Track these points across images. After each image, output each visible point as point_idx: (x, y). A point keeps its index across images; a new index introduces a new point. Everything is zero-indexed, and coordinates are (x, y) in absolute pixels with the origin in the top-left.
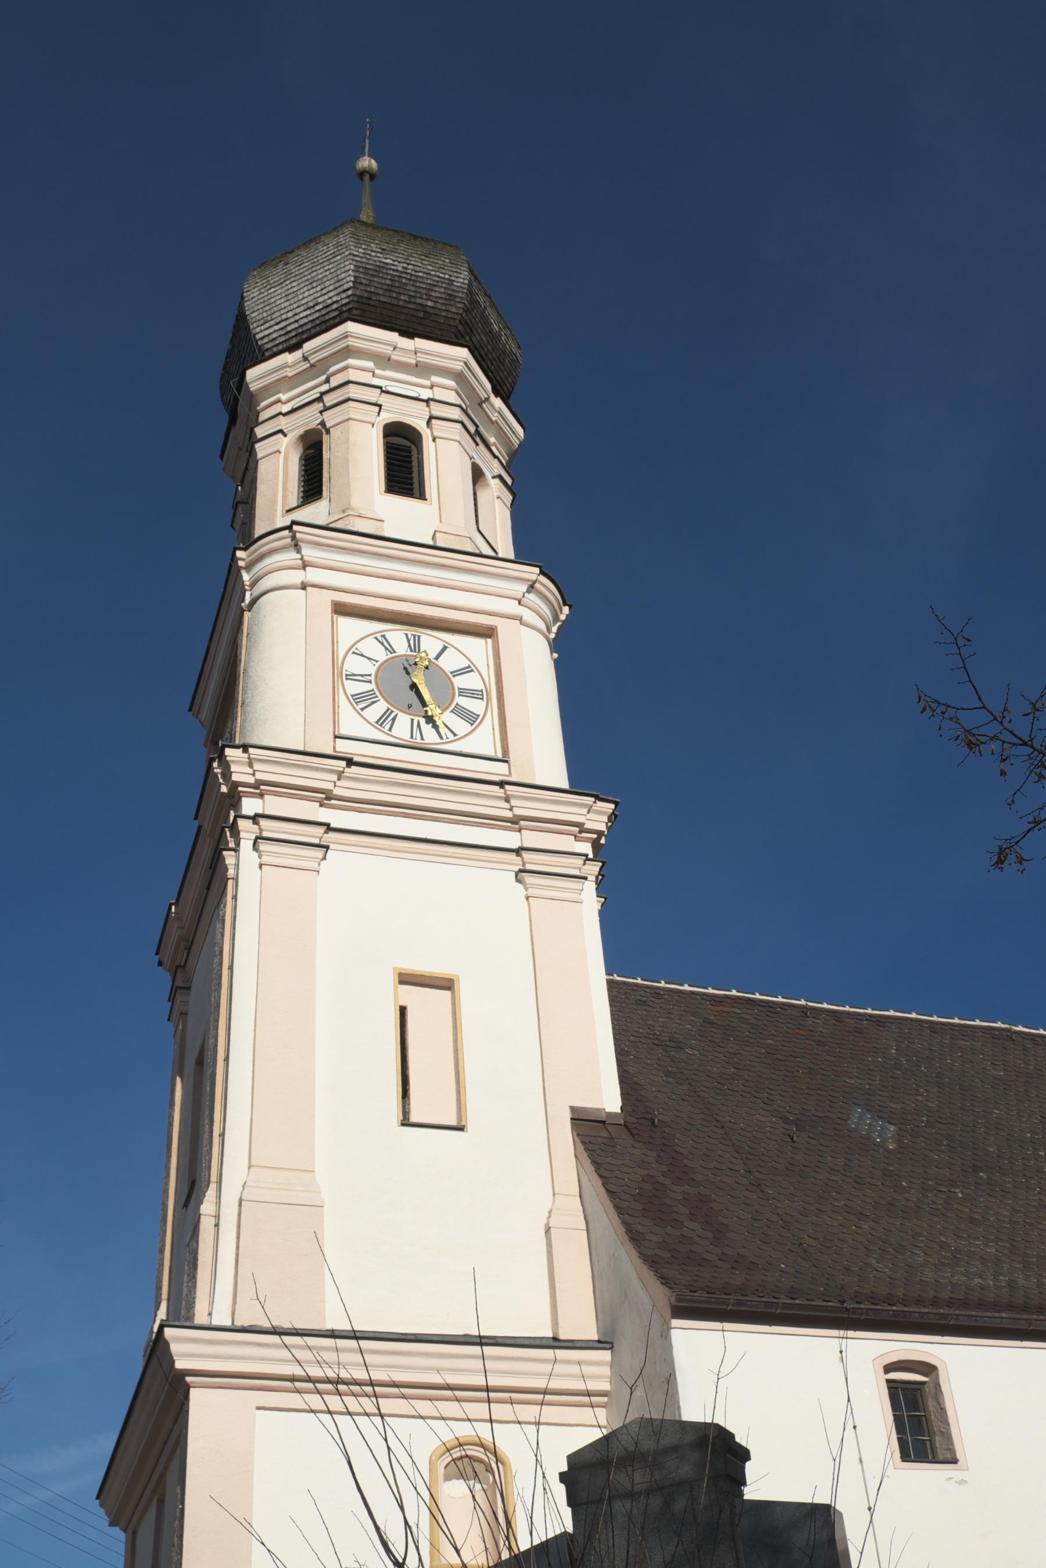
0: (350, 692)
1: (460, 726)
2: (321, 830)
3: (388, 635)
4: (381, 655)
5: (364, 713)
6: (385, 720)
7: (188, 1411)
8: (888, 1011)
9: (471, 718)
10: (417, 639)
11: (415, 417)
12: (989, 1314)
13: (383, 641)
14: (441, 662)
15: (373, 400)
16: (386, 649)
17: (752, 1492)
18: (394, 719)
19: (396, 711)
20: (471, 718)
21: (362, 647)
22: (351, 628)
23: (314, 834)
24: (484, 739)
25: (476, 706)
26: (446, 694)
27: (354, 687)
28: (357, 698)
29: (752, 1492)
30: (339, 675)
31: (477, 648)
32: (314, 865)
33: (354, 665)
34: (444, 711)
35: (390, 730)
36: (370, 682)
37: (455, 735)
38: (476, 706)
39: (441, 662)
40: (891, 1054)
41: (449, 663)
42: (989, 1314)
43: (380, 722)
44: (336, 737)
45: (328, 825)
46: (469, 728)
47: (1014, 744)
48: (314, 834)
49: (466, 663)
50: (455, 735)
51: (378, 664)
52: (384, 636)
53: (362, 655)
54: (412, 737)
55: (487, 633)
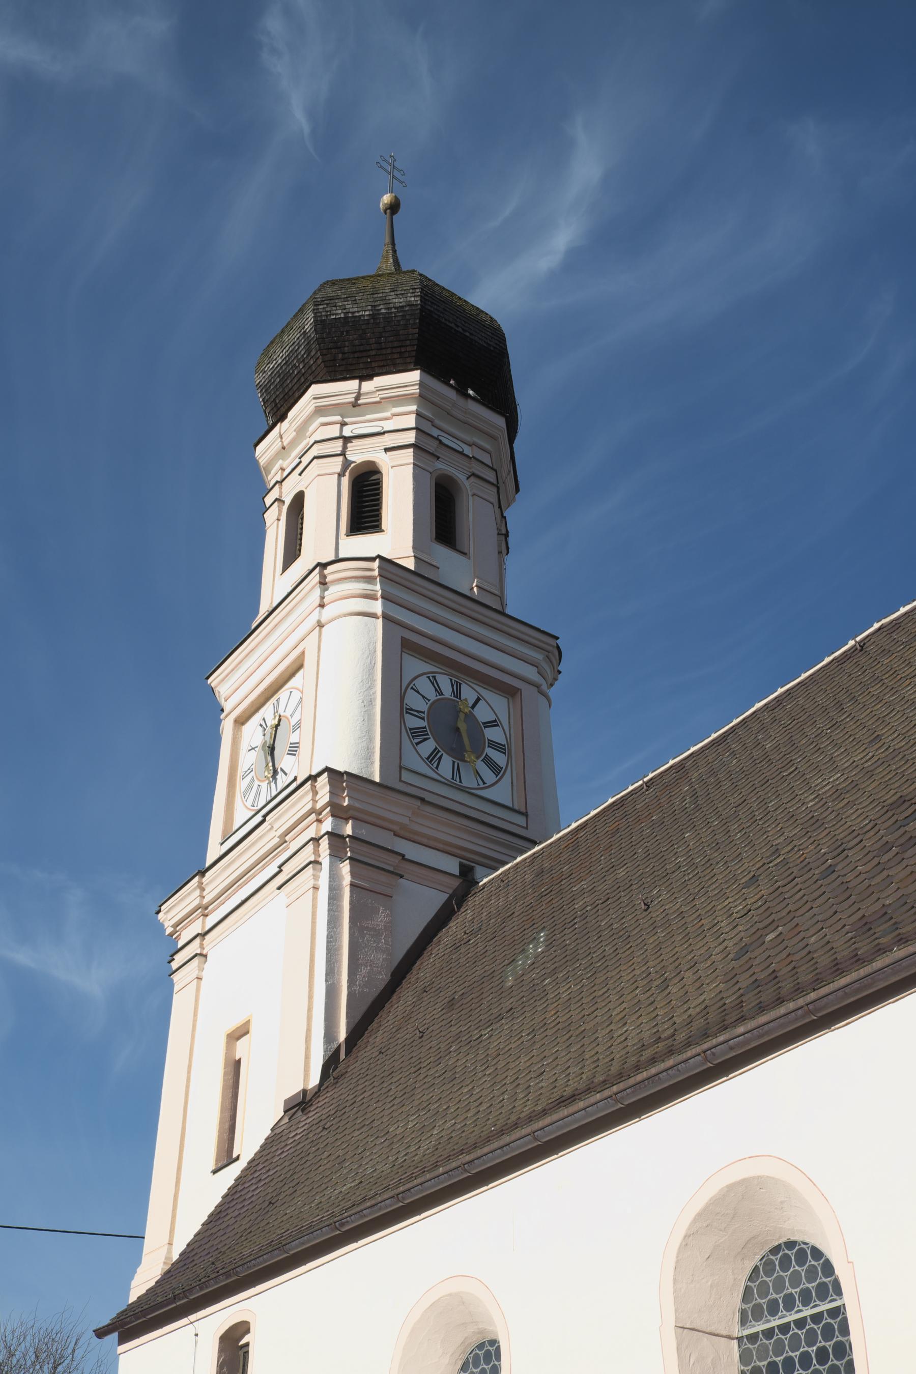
1: (489, 776)
2: (396, 860)
3: (438, 677)
4: (432, 695)
5: (419, 747)
6: (433, 758)
8: (899, 610)
10: (459, 686)
12: (721, 1038)
13: (434, 681)
15: (432, 450)
16: (436, 690)
18: (440, 758)
19: (442, 752)
23: (391, 862)
24: (502, 792)
25: (499, 758)
26: (479, 744)
27: (413, 722)
33: (414, 701)
34: (478, 758)
35: (417, 744)
36: (423, 719)
37: (484, 783)
40: (512, 975)
41: (482, 714)
42: (721, 1038)
44: (401, 768)
45: (403, 856)
48: (391, 862)
49: (493, 718)
50: (484, 783)
51: (429, 703)
52: (434, 677)
53: (423, 697)
54: (453, 778)
55: (510, 692)
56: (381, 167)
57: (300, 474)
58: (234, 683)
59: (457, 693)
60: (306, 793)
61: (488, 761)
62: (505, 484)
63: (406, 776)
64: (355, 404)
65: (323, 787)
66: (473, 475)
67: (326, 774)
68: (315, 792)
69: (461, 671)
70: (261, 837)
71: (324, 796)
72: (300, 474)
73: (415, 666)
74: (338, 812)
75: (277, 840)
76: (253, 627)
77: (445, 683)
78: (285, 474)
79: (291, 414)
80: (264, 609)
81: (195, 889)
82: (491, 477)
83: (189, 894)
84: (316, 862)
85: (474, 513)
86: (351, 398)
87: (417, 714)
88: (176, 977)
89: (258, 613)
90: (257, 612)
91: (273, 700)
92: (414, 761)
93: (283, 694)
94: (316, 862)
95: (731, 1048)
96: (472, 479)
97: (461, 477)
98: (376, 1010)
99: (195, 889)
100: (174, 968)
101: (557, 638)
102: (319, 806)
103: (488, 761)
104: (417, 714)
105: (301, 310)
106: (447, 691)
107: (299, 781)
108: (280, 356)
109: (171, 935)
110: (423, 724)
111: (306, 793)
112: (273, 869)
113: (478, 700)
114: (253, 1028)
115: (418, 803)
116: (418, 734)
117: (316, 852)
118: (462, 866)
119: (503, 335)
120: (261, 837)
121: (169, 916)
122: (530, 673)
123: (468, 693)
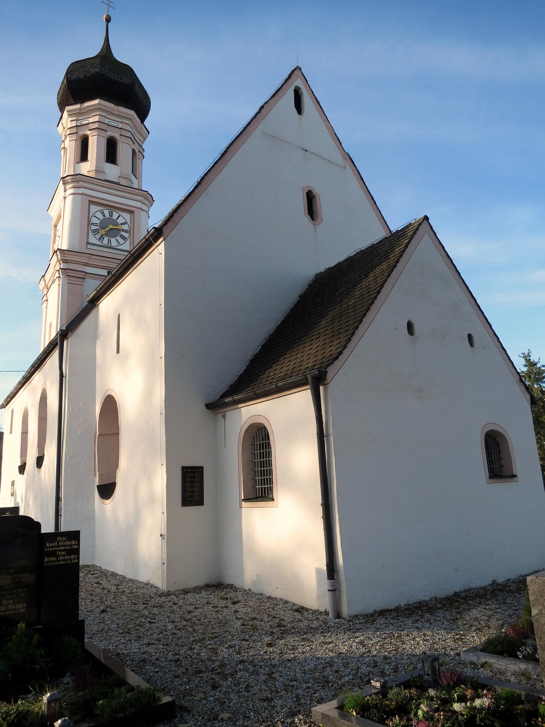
0: (92, 229)
1: (121, 241)
2: (83, 274)
4: (101, 217)
5: (96, 236)
7: (2, 444)
9: (124, 238)
11: (116, 135)
13: (102, 213)
14: (118, 221)
17: (42, 532)
20: (124, 238)
21: (96, 214)
22: (94, 209)
23: (81, 275)
25: (126, 235)
27: (93, 227)
28: (94, 231)
29: (42, 532)
30: (89, 223)
31: (127, 216)
32: (81, 283)
33: (94, 220)
38: (126, 235)
39: (118, 221)
43: (100, 239)
46: (124, 242)
47: (104, 3)
55: (131, 212)
56: (104, 3)
62: (138, 139)
63: (89, 246)
68: (57, 256)
69: (112, 208)
77: (107, 213)
84: (60, 277)
85: (124, 151)
92: (93, 239)
94: (60, 277)
95: (40, 461)
96: (122, 137)
97: (117, 136)
106: (107, 215)
108: (61, 93)
110: (98, 227)
116: (95, 232)
119: (73, 64)
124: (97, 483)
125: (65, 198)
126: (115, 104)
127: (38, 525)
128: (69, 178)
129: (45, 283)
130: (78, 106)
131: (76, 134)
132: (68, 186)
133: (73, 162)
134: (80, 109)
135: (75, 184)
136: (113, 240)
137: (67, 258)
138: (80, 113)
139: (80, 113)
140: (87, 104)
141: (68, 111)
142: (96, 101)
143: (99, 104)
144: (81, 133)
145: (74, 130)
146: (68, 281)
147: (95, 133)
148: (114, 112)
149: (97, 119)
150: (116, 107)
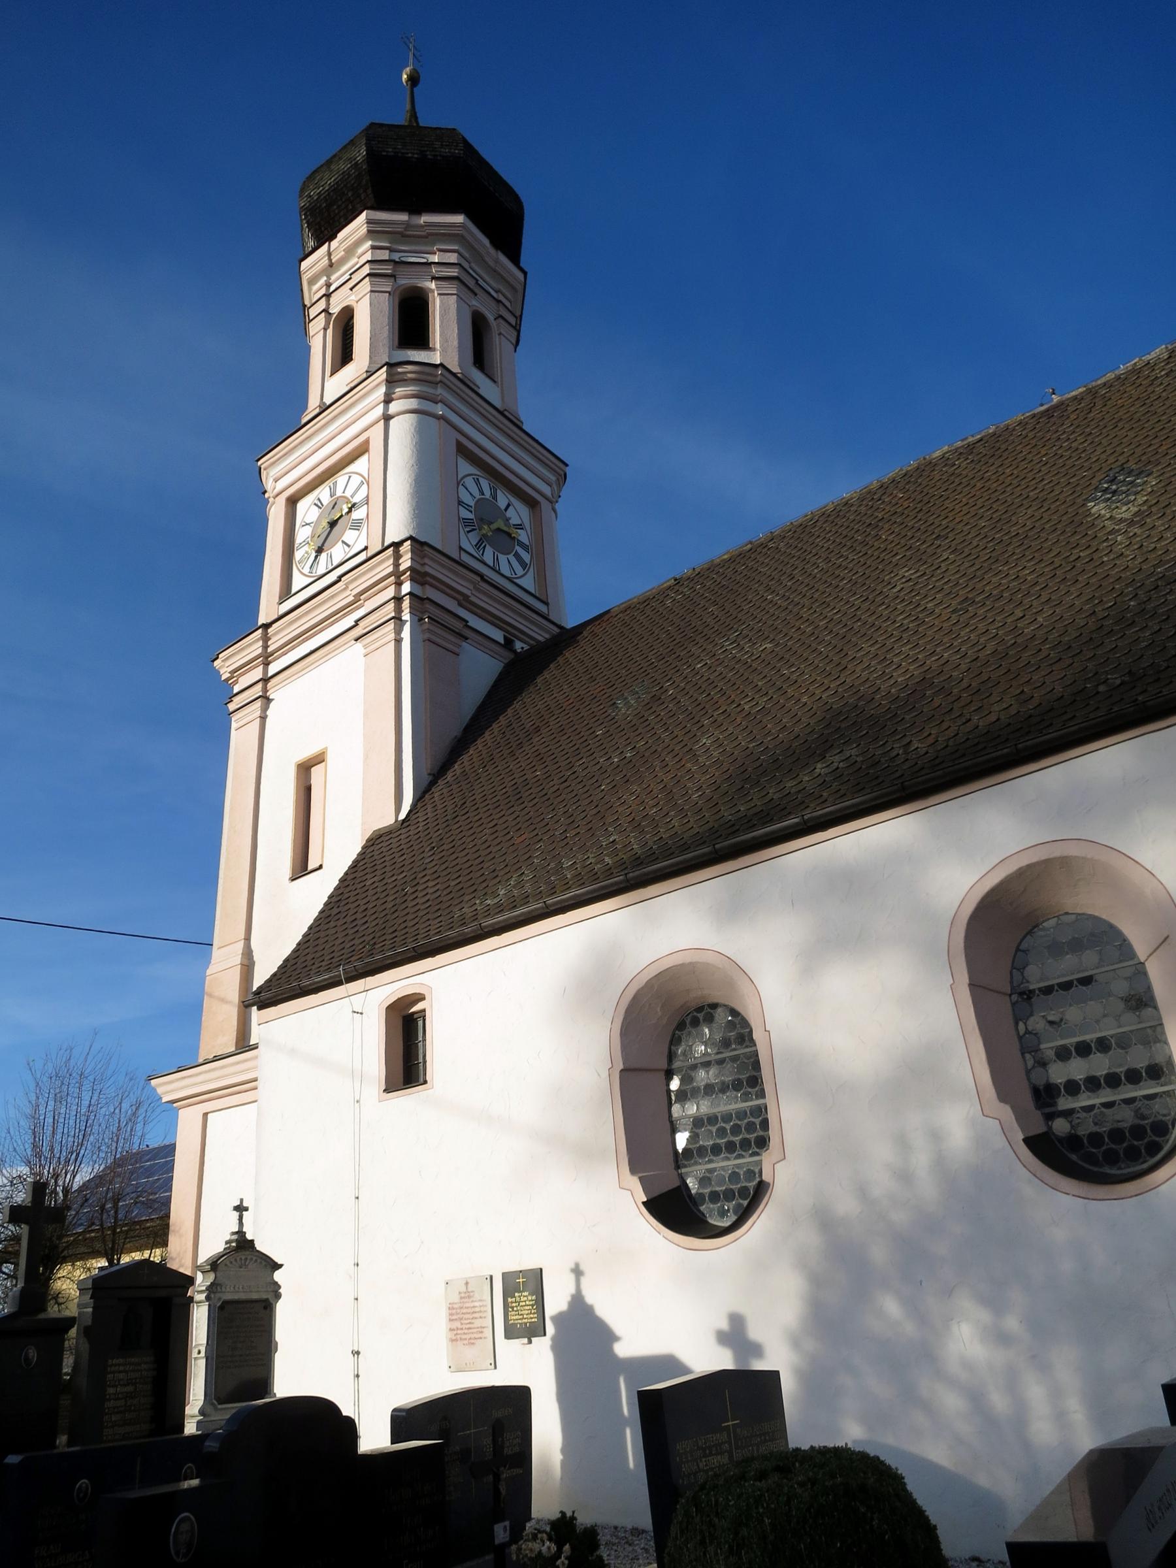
3: (481, 480)
13: (477, 482)
20: (357, 525)
23: (458, 625)
25: (526, 557)
48: (458, 625)
57: (351, 289)
58: (282, 472)
59: (495, 497)
60: (388, 558)
61: (517, 555)
64: (331, 265)
65: (406, 552)
66: (501, 317)
67: (409, 542)
70: (332, 597)
71: (406, 563)
72: (351, 289)
73: (465, 468)
74: (417, 575)
75: (351, 598)
76: (304, 420)
78: (332, 288)
79: (341, 235)
80: (313, 403)
81: (258, 640)
82: (513, 321)
83: (250, 645)
86: (325, 261)
87: (467, 507)
88: (234, 718)
89: (306, 408)
90: (305, 406)
91: (330, 483)
93: (341, 479)
97: (490, 317)
98: (455, 743)
99: (258, 640)
100: (231, 710)
101: (567, 465)
102: (402, 568)
103: (517, 555)
104: (467, 507)
105: (352, 143)
106: (487, 494)
107: (370, 552)
108: (329, 180)
109: (227, 680)
110: (471, 516)
111: (388, 558)
112: (348, 621)
113: (508, 505)
114: (330, 757)
115: (479, 579)
117: (398, 610)
118: (505, 638)
120: (332, 597)
121: (225, 666)
122: (546, 490)
123: (502, 501)
124: (1021, 1136)
125: (387, 418)
126: (492, 242)
127: (347, 1429)
128: (410, 368)
129: (265, 647)
130: (403, 217)
131: (392, 280)
132: (399, 391)
133: (386, 341)
134: (408, 225)
135: (424, 389)
136: (503, 558)
137: (427, 569)
138: (404, 236)
139: (404, 236)
140: (425, 219)
141: (369, 222)
142: (459, 219)
143: (463, 226)
144: (403, 281)
145: (387, 269)
146: (427, 635)
147: (452, 288)
148: (487, 259)
149: (453, 258)
150: (492, 251)
